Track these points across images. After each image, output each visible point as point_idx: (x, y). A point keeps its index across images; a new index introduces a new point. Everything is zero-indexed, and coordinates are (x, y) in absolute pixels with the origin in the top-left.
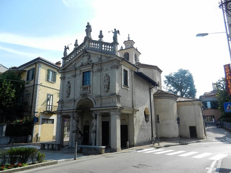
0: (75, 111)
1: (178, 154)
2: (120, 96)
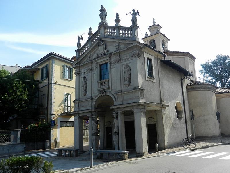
0: (93, 110)
1: (218, 156)
2: (144, 90)
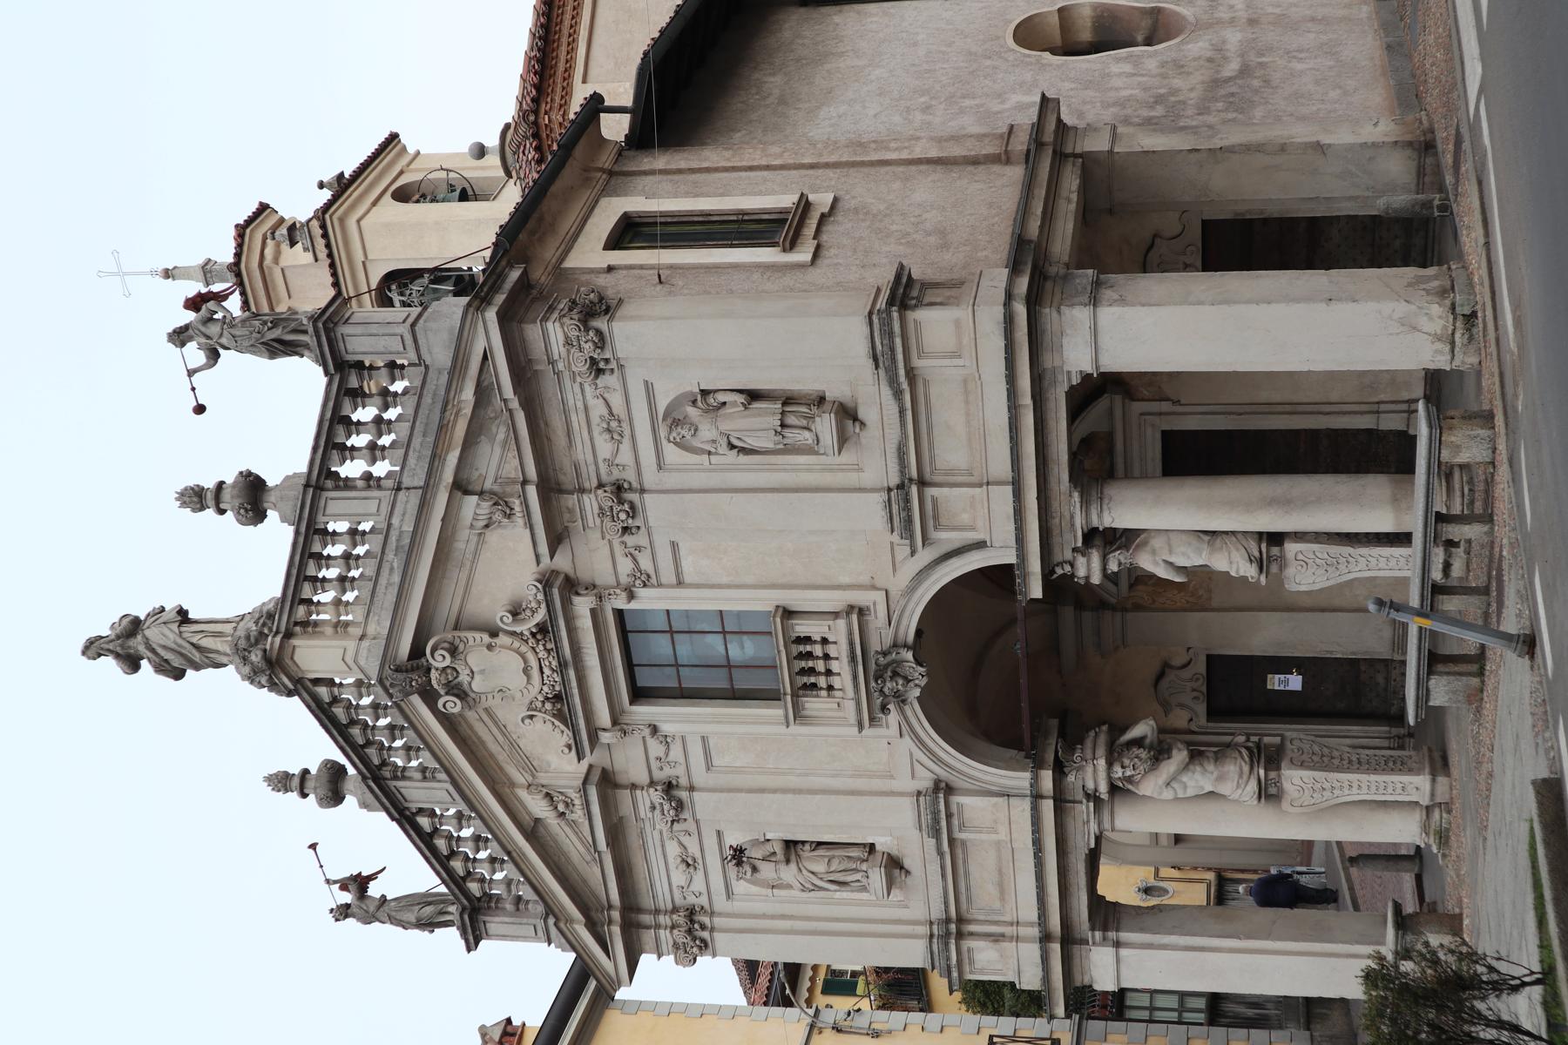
0: (1047, 778)
